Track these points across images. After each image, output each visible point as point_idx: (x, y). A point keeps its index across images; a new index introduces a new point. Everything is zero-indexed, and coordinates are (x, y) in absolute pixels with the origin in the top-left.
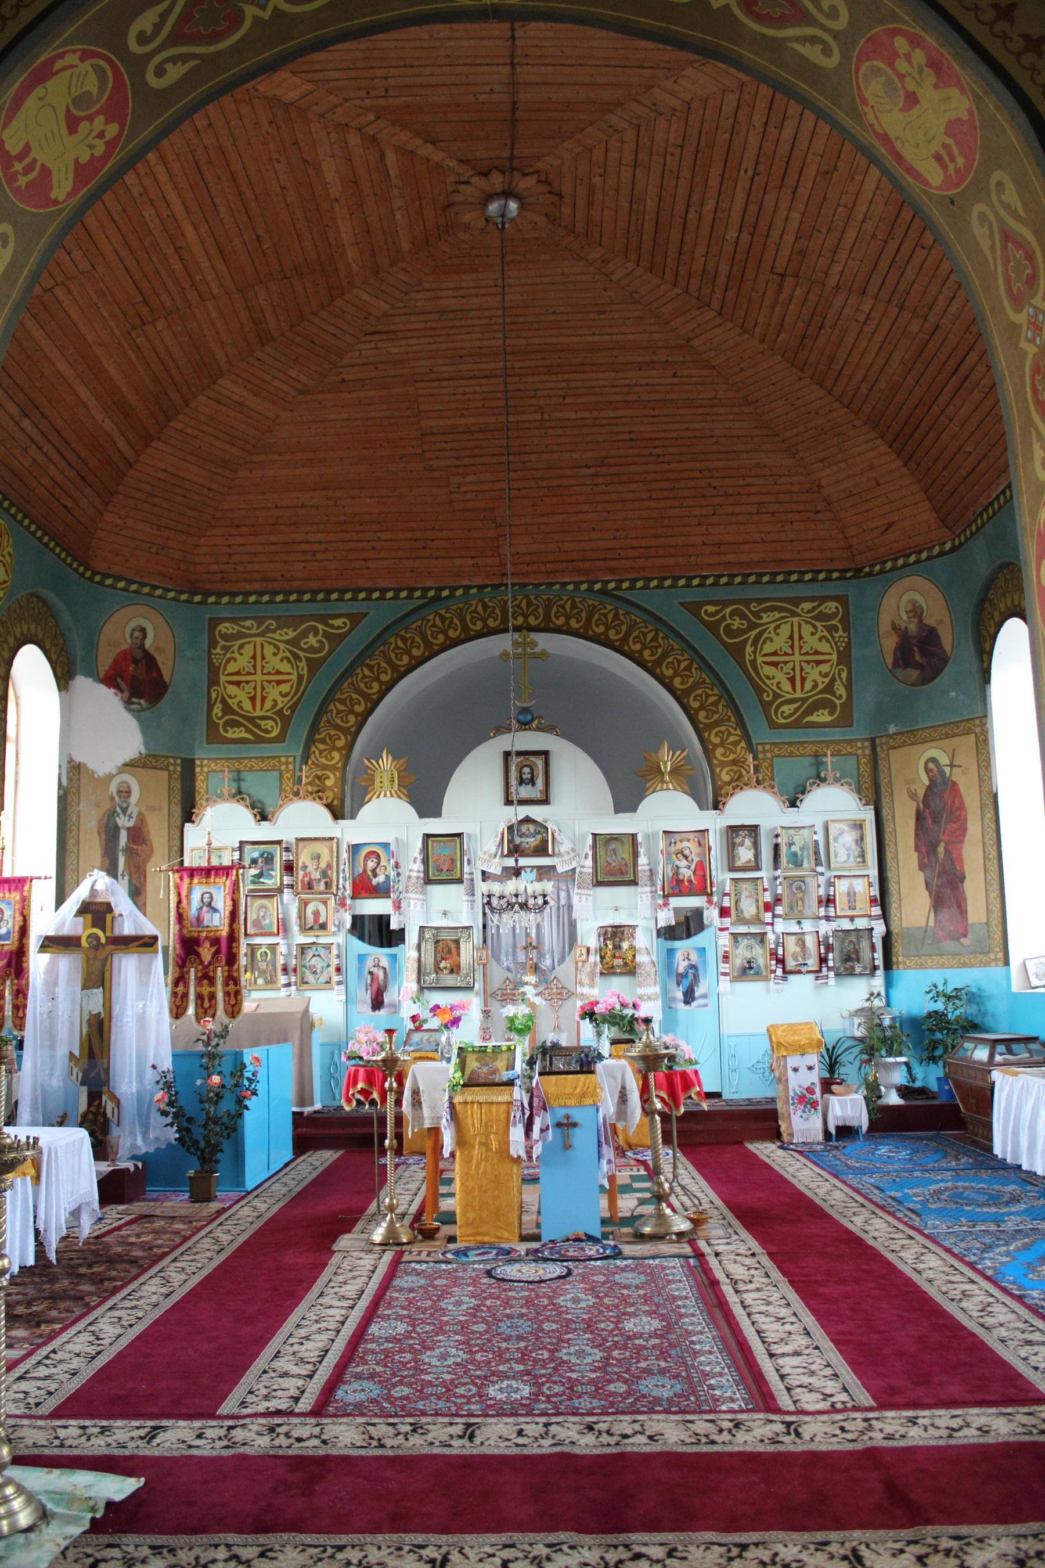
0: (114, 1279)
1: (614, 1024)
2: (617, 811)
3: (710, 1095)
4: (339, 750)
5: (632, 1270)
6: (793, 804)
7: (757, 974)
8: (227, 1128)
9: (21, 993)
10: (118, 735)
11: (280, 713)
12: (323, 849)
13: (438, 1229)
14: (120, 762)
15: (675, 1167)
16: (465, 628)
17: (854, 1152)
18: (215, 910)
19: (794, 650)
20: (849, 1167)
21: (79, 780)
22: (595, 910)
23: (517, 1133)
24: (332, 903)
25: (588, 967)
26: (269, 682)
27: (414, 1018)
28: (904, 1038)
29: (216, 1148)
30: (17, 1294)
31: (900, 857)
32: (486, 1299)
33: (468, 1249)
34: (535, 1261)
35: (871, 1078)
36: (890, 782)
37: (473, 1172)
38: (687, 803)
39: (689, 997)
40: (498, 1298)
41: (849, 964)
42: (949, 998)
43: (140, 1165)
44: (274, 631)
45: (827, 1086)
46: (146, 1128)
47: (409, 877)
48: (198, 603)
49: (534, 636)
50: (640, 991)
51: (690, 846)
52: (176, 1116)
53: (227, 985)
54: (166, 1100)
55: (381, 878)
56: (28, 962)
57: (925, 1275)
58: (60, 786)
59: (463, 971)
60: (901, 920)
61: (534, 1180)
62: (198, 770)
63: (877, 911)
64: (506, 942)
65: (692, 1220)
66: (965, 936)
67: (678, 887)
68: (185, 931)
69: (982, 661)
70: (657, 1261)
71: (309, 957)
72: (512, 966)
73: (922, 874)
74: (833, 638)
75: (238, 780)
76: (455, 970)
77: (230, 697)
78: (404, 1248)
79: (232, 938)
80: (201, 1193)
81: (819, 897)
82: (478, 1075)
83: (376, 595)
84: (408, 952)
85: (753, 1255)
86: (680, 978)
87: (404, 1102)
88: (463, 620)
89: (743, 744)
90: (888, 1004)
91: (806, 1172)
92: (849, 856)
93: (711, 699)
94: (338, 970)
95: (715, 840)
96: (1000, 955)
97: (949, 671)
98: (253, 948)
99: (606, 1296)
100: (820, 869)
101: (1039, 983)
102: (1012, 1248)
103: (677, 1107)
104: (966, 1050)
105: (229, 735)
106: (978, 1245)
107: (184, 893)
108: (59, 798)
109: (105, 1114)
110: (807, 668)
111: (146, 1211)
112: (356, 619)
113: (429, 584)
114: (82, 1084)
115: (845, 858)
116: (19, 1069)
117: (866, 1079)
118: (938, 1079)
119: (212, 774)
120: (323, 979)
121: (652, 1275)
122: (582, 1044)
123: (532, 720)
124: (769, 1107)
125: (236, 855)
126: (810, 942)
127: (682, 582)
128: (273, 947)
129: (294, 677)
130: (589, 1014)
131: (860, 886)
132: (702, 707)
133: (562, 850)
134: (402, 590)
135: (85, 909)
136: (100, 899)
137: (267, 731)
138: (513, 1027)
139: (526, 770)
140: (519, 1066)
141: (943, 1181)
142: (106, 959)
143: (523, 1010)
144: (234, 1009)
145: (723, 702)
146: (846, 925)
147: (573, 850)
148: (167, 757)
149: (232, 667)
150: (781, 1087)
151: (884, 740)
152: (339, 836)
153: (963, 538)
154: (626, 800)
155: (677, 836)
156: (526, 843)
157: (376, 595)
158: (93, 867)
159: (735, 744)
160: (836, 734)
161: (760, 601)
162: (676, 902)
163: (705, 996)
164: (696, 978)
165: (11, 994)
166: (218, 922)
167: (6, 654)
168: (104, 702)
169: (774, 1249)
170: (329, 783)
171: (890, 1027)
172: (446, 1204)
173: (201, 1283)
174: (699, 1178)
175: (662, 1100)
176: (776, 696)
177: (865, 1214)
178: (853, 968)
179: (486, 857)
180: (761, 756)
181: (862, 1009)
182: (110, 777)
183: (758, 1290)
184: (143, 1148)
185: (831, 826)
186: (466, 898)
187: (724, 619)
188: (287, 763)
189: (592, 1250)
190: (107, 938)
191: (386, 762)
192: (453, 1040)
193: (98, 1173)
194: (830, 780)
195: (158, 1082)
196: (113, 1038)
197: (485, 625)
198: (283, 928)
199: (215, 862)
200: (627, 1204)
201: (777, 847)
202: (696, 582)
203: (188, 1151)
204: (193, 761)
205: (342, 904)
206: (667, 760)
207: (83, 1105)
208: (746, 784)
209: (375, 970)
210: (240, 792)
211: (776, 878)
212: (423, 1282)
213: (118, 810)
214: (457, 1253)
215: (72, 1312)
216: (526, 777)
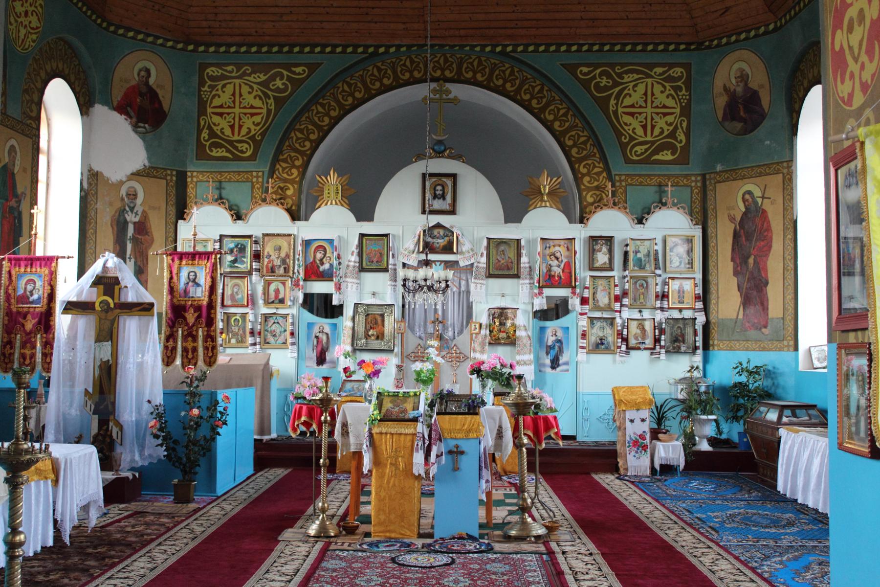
0: (112, 557)
1: (494, 379)
2: (506, 222)
3: (565, 438)
4: (297, 168)
5: (500, 562)
6: (640, 221)
7: (607, 348)
8: (203, 449)
9: (48, 344)
10: (128, 152)
11: (252, 138)
12: (283, 243)
13: (357, 527)
14: (129, 173)
15: (536, 487)
16: (396, 77)
17: (672, 484)
18: (198, 285)
19: (647, 104)
20: (668, 495)
21: (96, 184)
22: (487, 296)
23: (419, 458)
24: (289, 283)
25: (480, 338)
26: (245, 114)
27: (346, 370)
28: (715, 401)
29: (195, 464)
30: (39, 566)
32: (389, 578)
33: (379, 542)
34: (428, 552)
35: (689, 431)
36: (715, 207)
37: (385, 485)
38: (561, 218)
39: (555, 364)
40: (399, 578)
42: (751, 373)
43: (137, 475)
44: (250, 75)
45: (655, 434)
46: (142, 447)
47: (348, 266)
48: (191, 51)
49: (449, 86)
50: (518, 358)
51: (561, 251)
52: (165, 438)
53: (206, 342)
54: (158, 426)
55: (327, 266)
56: (54, 321)
57: (717, 575)
58: (82, 189)
59: (386, 338)
60: (717, 312)
61: (431, 494)
62: (189, 180)
63: (700, 305)
64: (419, 316)
65: (547, 527)
66: (765, 327)
67: (550, 281)
68: (175, 300)
69: (792, 118)
70: (519, 556)
71: (270, 324)
72: (423, 335)
73: (735, 279)
74: (678, 95)
75: (220, 188)
76: (380, 336)
77: (214, 124)
78: (332, 540)
79: (211, 306)
80: (183, 496)
81: (657, 293)
82: (393, 411)
83: (328, 49)
84: (345, 322)
85: (591, 554)
86: (549, 349)
87: (336, 432)
88: (395, 72)
89: (604, 174)
90: (705, 375)
91: (635, 496)
92: (680, 262)
93: (582, 139)
94: (292, 334)
95: (579, 247)
96: (792, 343)
97: (766, 124)
98: (228, 316)
99: (479, 579)
100: (658, 272)
101: (819, 365)
102: (784, 559)
103: (540, 443)
104: (761, 413)
105: (214, 154)
106: (760, 555)
107: (175, 271)
108: (81, 198)
109: (111, 436)
111: (140, 509)
112: (312, 68)
113: (369, 43)
114: (94, 413)
115: (678, 264)
116: (46, 401)
117: (684, 431)
118: (739, 433)
119: (200, 182)
120: (281, 340)
121: (514, 565)
122: (473, 393)
123: (445, 150)
124: (611, 448)
125: (217, 246)
126: (648, 326)
127: (563, 48)
128: (244, 316)
129: (264, 111)
130: (477, 371)
131: (688, 286)
132: (575, 145)
133: (464, 249)
134: (348, 46)
135: (98, 281)
136: (110, 274)
137: (242, 152)
138: (422, 380)
139: (439, 188)
140: (422, 408)
141: (738, 508)
142: (114, 320)
143: (428, 366)
144: (211, 360)
145: (591, 142)
146: (676, 315)
147: (472, 250)
148: (166, 170)
149: (217, 102)
150: (620, 433)
151: (713, 176)
152: (296, 233)
153: (783, 21)
154: (514, 215)
155: (551, 243)
156: (437, 243)
157: (328, 49)
158: (105, 250)
160: (676, 170)
161: (623, 65)
162: (548, 292)
163: (567, 363)
164: (561, 350)
165: (41, 345)
166: (200, 294)
167: (39, 85)
168: (117, 126)
169: (606, 550)
170: (289, 193)
171: (705, 393)
172: (365, 510)
173: (178, 562)
174: (555, 497)
175: (529, 437)
176: (632, 139)
177: (677, 529)
178: (679, 348)
179: (406, 253)
180: (618, 184)
181: (685, 379)
182: (122, 183)
183: (592, 579)
184: (139, 462)
185: (669, 240)
186: (389, 283)
187: (594, 77)
188: (257, 177)
189: (471, 546)
190: (115, 304)
191: (333, 179)
192: (374, 387)
193: (103, 480)
194: (669, 204)
195: (152, 413)
196: (118, 379)
197: (412, 76)
198: (251, 301)
199: (200, 248)
200: (499, 514)
201: (626, 254)
202: (574, 48)
203: (173, 465)
204: (186, 172)
205: (296, 284)
206: (546, 184)
207: (95, 429)
208: (605, 205)
209: (320, 335)
210: (221, 198)
211: (624, 277)
212: (344, 564)
213: (127, 209)
214: (371, 545)
215: (79, 580)
216: (440, 193)
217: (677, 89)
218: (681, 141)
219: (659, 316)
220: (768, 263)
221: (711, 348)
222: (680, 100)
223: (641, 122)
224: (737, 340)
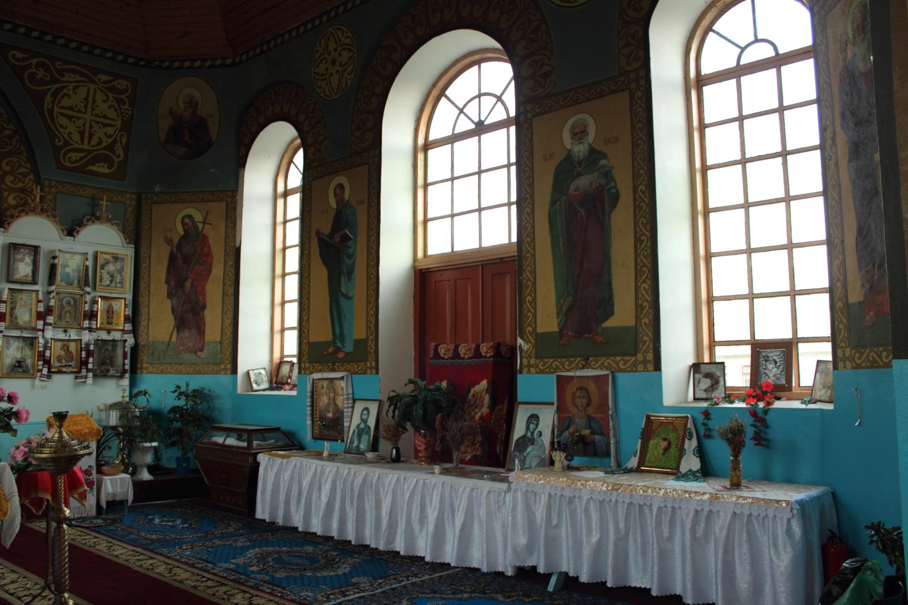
7: (24, 372)
31: (152, 287)
36: (150, 228)
41: (104, 367)
60: (148, 334)
63: (128, 327)
66: (201, 350)
74: (120, 109)
89: (32, 176)
96: (650, 356)
100: (88, 289)
110: (96, 127)
146: (104, 335)
151: (150, 196)
153: (244, 57)
159: (25, 175)
176: (67, 143)
178: (108, 370)
180: (47, 189)
211: (50, 293)
217: (120, 102)
218: (119, 156)
219: (86, 337)
220: (207, 287)
221: (139, 371)
222: (122, 114)
223: (79, 127)
224: (170, 363)
